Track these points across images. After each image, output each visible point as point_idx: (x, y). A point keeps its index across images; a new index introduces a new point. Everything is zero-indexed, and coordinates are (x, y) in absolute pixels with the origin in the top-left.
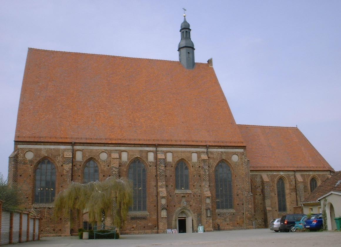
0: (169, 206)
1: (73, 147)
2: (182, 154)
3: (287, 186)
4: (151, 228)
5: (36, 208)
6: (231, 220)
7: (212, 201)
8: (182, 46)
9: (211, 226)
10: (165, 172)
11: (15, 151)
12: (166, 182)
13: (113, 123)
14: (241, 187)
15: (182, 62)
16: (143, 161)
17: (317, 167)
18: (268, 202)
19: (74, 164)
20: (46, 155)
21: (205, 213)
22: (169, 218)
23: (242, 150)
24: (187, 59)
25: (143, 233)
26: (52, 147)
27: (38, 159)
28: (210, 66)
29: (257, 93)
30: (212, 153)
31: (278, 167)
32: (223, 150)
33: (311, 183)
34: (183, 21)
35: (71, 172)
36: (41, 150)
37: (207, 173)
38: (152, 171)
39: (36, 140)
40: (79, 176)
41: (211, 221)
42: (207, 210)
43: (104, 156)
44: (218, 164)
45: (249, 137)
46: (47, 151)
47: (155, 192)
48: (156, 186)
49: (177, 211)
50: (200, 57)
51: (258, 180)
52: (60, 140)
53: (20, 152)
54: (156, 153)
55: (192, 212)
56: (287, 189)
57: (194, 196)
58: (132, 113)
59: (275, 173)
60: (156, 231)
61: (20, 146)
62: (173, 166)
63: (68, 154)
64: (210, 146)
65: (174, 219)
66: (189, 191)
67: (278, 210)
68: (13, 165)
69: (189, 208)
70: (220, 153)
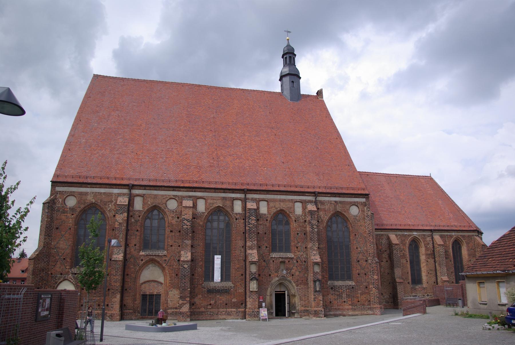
0: (261, 276)
1: (130, 191)
2: (282, 204)
3: (422, 250)
4: (236, 306)
5: (75, 274)
6: (348, 296)
7: (323, 270)
8: (283, 74)
9: (321, 305)
10: (256, 227)
11: (51, 195)
12: (258, 241)
13: (188, 161)
14: (363, 250)
15: (285, 93)
16: (227, 211)
17: (460, 226)
18: (398, 272)
19: (131, 214)
20: (94, 201)
21: (312, 286)
22: (261, 292)
23: (363, 200)
24: (291, 89)
25: (224, 313)
26: (102, 190)
27: (82, 206)
28: (320, 99)
29: (389, 110)
30: (322, 203)
31: (409, 225)
32: (337, 199)
33: (453, 247)
34: (286, 45)
35: (125, 225)
36: (86, 194)
37: (316, 230)
38: (239, 226)
39: (81, 180)
40: (138, 230)
41: (321, 298)
42: (315, 282)
43: (172, 205)
44: (330, 218)
45: (367, 189)
46: (95, 194)
47: (243, 254)
48: (245, 247)
49: (273, 281)
50: (308, 86)
51: (384, 241)
52: (114, 182)
53: (58, 196)
54: (244, 201)
55: (294, 284)
56: (423, 255)
57: (297, 261)
58: (216, 149)
59: (406, 233)
60: (243, 310)
61: (58, 189)
62: (269, 219)
63: (122, 201)
64: (319, 193)
65: (268, 294)
66: (290, 255)
67: (410, 283)
68: (46, 214)
69: (290, 278)
70: (334, 203)
